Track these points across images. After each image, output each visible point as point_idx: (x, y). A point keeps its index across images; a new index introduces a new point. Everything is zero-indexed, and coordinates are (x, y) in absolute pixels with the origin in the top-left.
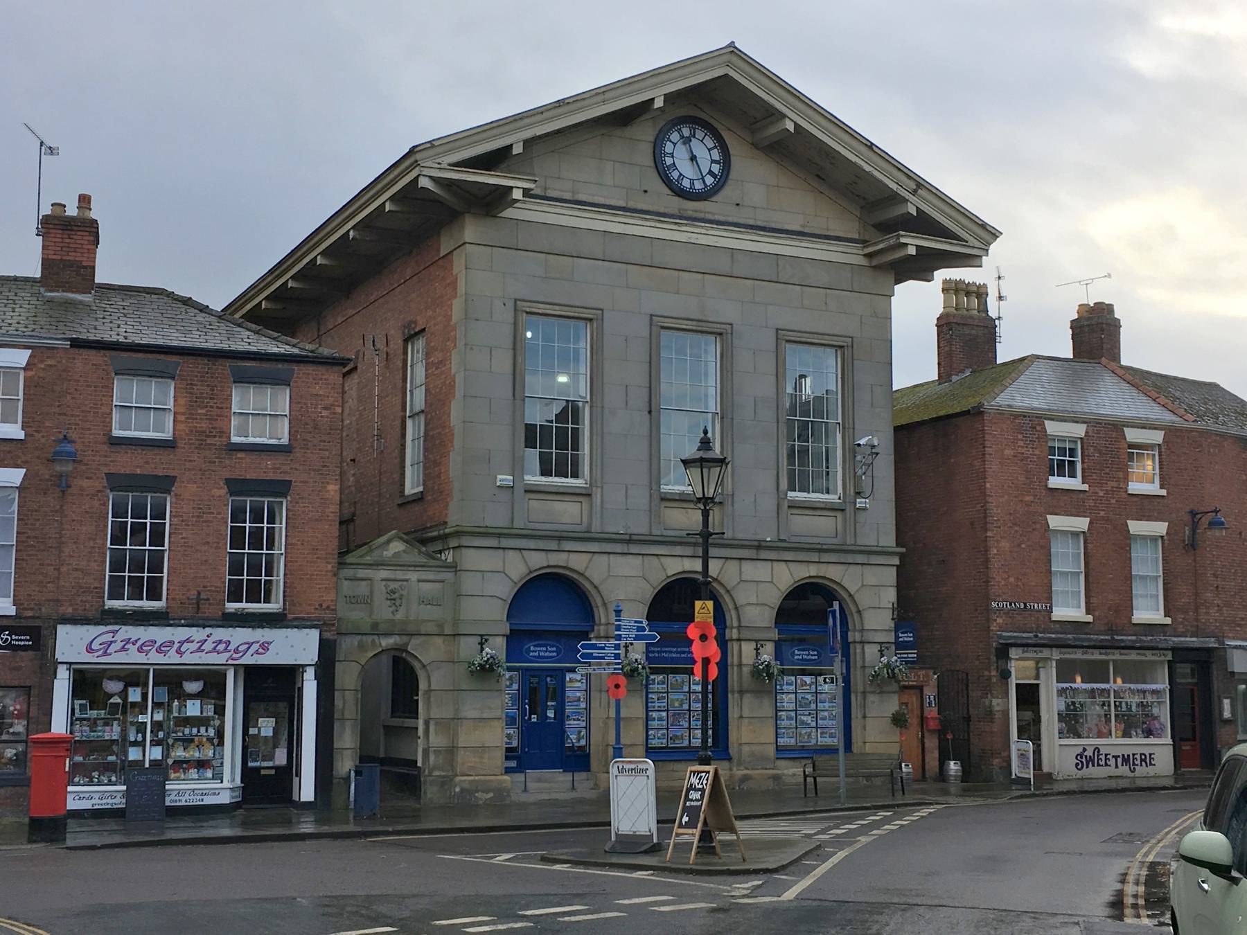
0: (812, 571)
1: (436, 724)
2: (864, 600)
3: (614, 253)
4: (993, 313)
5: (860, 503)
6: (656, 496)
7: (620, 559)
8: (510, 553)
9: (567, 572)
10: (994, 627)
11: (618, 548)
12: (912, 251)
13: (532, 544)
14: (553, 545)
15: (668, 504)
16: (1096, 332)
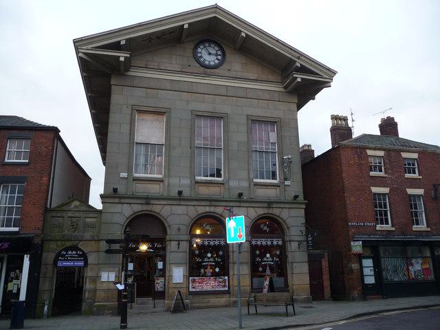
0: (208, 209)
1: (90, 279)
2: (290, 222)
3: (176, 88)
4: (350, 126)
5: (287, 183)
6: (193, 183)
7: (177, 207)
8: (125, 205)
9: (136, 214)
10: (350, 233)
11: (175, 202)
12: (299, 80)
13: (135, 201)
14: (208, 203)
15: (198, 184)
16: (389, 126)
